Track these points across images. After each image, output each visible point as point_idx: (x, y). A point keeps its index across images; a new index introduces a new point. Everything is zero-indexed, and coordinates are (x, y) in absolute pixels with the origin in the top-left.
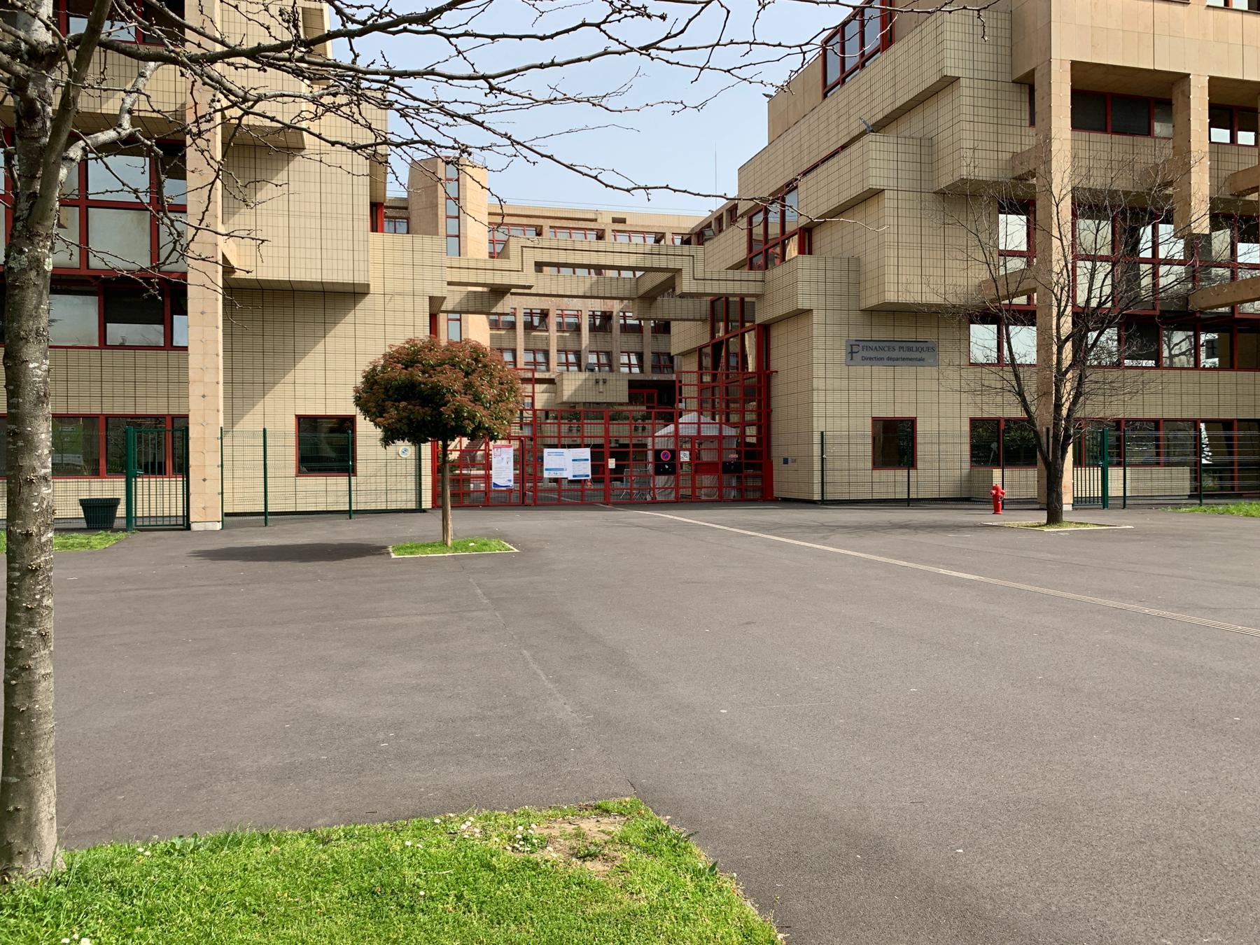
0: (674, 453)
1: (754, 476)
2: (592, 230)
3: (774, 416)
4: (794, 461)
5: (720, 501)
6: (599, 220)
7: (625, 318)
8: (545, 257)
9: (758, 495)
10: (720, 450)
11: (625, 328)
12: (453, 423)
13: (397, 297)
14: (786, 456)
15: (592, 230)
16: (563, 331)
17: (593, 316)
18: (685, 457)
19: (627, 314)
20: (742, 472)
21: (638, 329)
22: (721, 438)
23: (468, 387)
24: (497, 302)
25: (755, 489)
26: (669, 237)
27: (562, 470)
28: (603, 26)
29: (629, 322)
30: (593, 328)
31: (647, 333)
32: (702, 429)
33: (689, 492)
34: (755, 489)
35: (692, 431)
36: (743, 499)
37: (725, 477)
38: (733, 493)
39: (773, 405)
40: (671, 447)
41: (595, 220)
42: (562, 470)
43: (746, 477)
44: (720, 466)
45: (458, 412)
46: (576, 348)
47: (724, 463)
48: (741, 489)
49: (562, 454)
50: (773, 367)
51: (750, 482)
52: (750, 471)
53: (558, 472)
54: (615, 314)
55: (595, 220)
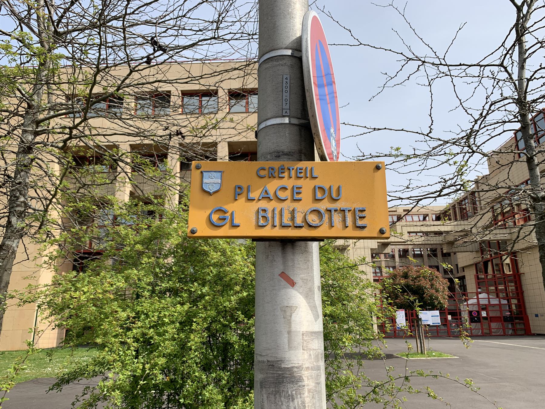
0: (479, 313)
1: (519, 323)
2: (395, 215)
3: (525, 294)
4: (542, 316)
5: (504, 336)
6: (398, 211)
7: (414, 251)
8: (412, 229)
9: (523, 332)
10: (501, 311)
11: (415, 256)
12: (429, 301)
13: (358, 250)
14: (536, 313)
15: (395, 215)
16: (387, 258)
17: (399, 251)
18: (484, 314)
19: (415, 250)
20: (514, 321)
21: (421, 256)
22: (500, 305)
23: (432, 285)
24: (385, 249)
25: (521, 329)
26: (430, 215)
27: (427, 320)
28: (231, 111)
29: (416, 253)
30: (400, 256)
31: (426, 257)
32: (491, 301)
33: (488, 331)
34: (521, 329)
35: (486, 302)
36: (516, 334)
37: (505, 324)
38: (510, 332)
39: (524, 288)
40: (477, 310)
41: (396, 211)
42: (427, 320)
43: (516, 323)
44: (502, 318)
45: (431, 296)
46: (393, 265)
47: (504, 317)
48: (514, 330)
49: (426, 314)
50: (521, 271)
51: (518, 326)
52: (517, 321)
53: (426, 322)
54: (410, 250)
55: (396, 211)
